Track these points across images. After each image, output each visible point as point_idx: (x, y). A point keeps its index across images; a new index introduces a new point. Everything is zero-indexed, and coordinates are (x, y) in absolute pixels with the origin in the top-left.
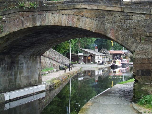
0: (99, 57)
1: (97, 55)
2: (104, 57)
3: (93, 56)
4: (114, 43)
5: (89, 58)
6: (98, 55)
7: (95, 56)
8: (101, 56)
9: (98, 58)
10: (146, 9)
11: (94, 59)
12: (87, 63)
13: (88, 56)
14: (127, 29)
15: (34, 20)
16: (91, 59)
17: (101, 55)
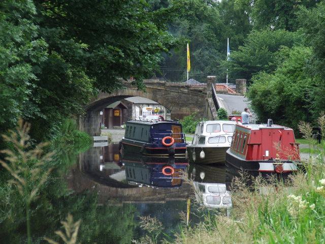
0: (144, 109)
1: (138, 104)
2: (159, 108)
3: (126, 107)
4: (203, 50)
5: (117, 114)
6: (139, 104)
7: (133, 107)
8: (150, 107)
9: (141, 112)
10: (177, 90)
11: (131, 115)
12: (110, 125)
13: (114, 108)
14: (168, 99)
15: (117, 92)
16: (121, 115)
17: (148, 105)
